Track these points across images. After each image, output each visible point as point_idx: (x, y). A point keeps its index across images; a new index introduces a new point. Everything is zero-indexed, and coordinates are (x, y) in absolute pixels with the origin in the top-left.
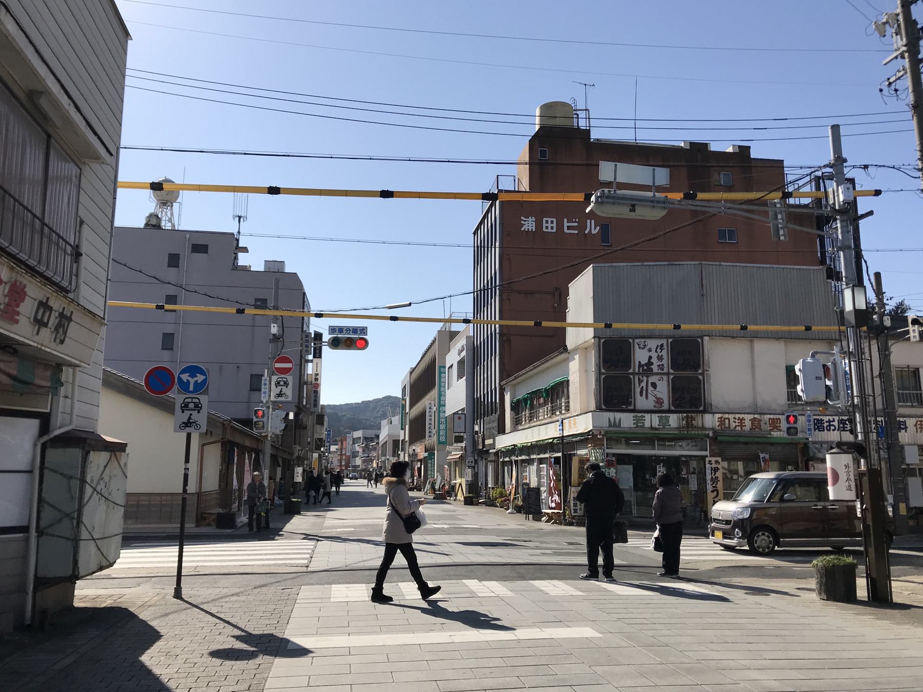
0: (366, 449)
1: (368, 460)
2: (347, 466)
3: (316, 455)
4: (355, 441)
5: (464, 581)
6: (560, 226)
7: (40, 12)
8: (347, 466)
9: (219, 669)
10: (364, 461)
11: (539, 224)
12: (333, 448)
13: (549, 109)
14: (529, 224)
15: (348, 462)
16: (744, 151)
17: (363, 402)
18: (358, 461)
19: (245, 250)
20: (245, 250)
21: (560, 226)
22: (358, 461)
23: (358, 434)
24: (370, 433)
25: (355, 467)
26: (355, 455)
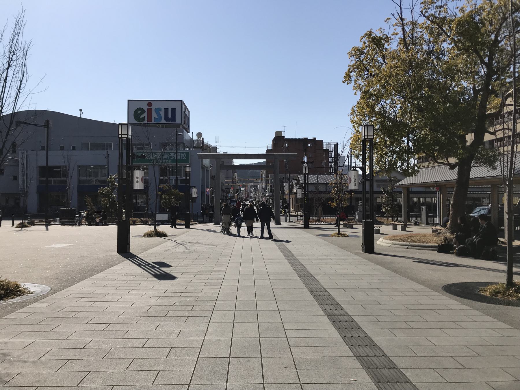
0: (255, 190)
1: (255, 194)
2: (248, 196)
4: (251, 187)
8: (248, 196)
12: (242, 189)
18: (252, 194)
22: (252, 194)
23: (252, 184)
24: (256, 184)
26: (251, 192)
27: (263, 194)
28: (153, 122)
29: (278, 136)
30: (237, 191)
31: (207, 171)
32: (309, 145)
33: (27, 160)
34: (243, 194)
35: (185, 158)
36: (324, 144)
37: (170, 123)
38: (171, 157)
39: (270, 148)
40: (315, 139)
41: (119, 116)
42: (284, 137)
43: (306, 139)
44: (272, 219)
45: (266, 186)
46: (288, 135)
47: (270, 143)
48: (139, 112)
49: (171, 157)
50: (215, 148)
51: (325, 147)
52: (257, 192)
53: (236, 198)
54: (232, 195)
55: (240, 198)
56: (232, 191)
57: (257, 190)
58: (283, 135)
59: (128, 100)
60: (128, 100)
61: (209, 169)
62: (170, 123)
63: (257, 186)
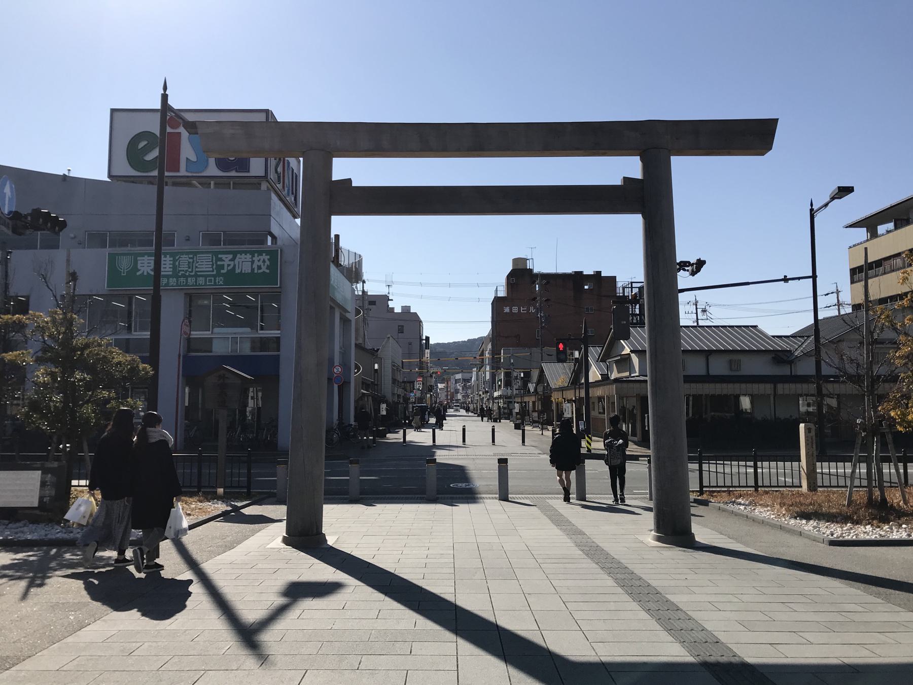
0: (465, 388)
1: (466, 396)
3: (428, 395)
4: (457, 381)
5: (690, 659)
6: (519, 310)
7: (7, 200)
8: (452, 400)
9: (376, 553)
10: (463, 396)
11: (511, 310)
12: (440, 386)
13: (516, 261)
14: (507, 310)
15: (452, 396)
16: (599, 273)
17: (469, 340)
18: (460, 396)
21: (519, 310)
22: (460, 396)
23: (459, 376)
24: (467, 376)
25: (458, 400)
26: (457, 391)
27: (487, 392)
28: (183, 172)
29: (520, 267)
30: (431, 389)
31: (345, 321)
32: (586, 287)
33: (763, 523)
34: (442, 397)
35: (264, 269)
36: (619, 285)
37: (233, 173)
38: (222, 267)
39: (502, 293)
40: (599, 273)
41: (84, 155)
42: (531, 270)
43: (579, 274)
44: (419, 437)
45: (493, 376)
46: (541, 266)
47: (502, 280)
48: (142, 144)
49: (222, 267)
50: (386, 298)
51: (620, 292)
52: (469, 391)
53: (429, 402)
54: (418, 394)
55: (436, 402)
56: (418, 385)
57: (470, 387)
59: (113, 111)
60: (113, 111)
61: (351, 316)
62: (233, 173)
63: (469, 380)
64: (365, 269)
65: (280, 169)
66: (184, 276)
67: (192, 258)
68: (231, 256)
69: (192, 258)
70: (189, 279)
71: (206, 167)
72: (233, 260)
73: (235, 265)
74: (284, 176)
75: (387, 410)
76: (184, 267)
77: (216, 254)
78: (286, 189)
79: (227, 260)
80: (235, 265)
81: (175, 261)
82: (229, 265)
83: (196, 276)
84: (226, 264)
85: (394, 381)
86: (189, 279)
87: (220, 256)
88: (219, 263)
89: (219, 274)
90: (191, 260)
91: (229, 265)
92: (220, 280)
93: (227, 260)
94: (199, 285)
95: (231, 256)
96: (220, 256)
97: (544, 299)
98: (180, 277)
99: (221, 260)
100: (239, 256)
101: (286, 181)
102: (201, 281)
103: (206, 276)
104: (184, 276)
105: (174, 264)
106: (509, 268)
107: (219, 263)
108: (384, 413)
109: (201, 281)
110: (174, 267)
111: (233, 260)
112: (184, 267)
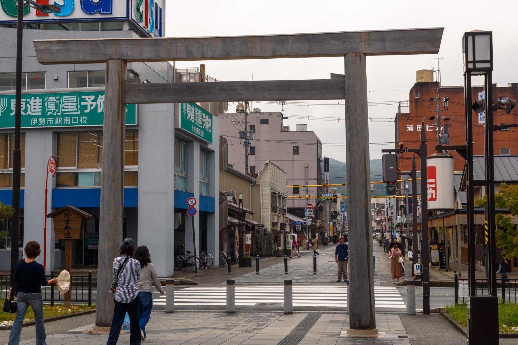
11: (415, 128)
14: (411, 128)
19: (286, 118)
20: (286, 118)
37: (98, 16)
38: (85, 107)
39: (406, 110)
49: (85, 107)
58: (436, 78)
64: (3, 305)
65: (142, 8)
66: (51, 116)
67: (59, 99)
68: (93, 97)
69: (59, 99)
70: (57, 119)
71: (73, 11)
72: (95, 100)
73: (97, 106)
74: (146, 13)
75: (252, 239)
76: (52, 108)
77: (79, 94)
78: (149, 25)
79: (90, 101)
80: (97, 106)
81: (43, 102)
82: (91, 106)
83: (63, 116)
84: (88, 104)
85: (274, 209)
86: (57, 119)
87: (83, 97)
88: (83, 103)
89: (83, 114)
90: (58, 102)
91: (91, 106)
92: (84, 120)
93: (90, 101)
94: (66, 124)
95: (93, 97)
96: (83, 97)
97: (444, 118)
98: (49, 117)
99: (84, 100)
100: (100, 96)
101: (149, 17)
102: (67, 120)
103: (71, 116)
104: (51, 116)
105: (43, 105)
106: (413, 81)
107: (83, 103)
108: (249, 242)
109: (67, 120)
110: (43, 108)
111: (95, 100)
112: (52, 108)
